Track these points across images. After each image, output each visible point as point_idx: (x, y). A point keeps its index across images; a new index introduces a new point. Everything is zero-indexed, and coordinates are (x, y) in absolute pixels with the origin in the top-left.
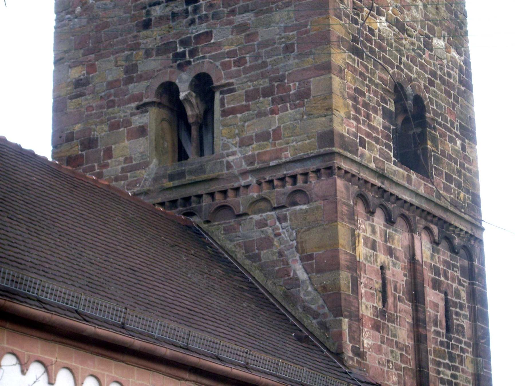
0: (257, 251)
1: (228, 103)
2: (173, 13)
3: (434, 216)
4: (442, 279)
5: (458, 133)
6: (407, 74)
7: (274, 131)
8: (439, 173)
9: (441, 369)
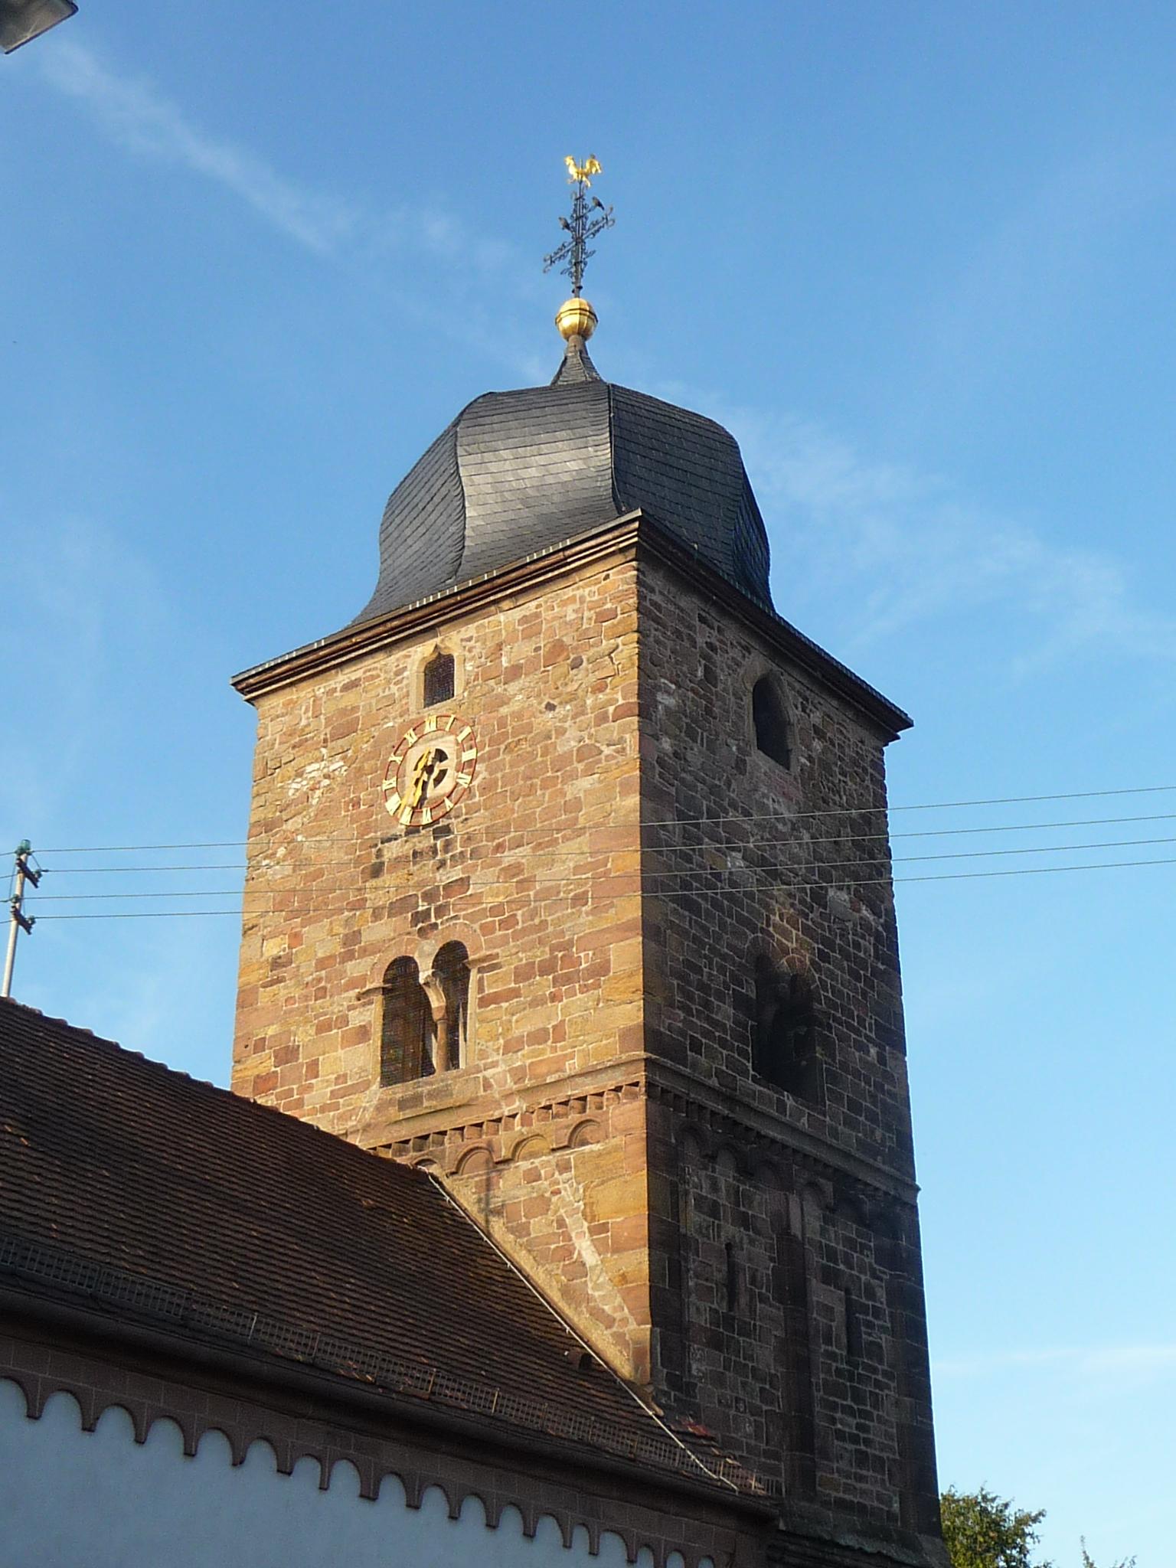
0: (524, 1220)
1: (490, 987)
2: (415, 853)
3: (826, 1166)
4: (842, 1267)
5: (873, 1035)
6: (780, 943)
7: (554, 1027)
8: (838, 1098)
9: (838, 1415)
